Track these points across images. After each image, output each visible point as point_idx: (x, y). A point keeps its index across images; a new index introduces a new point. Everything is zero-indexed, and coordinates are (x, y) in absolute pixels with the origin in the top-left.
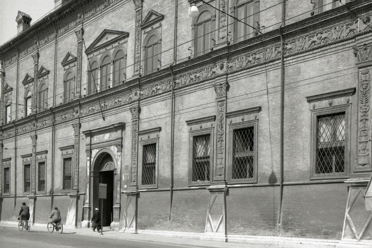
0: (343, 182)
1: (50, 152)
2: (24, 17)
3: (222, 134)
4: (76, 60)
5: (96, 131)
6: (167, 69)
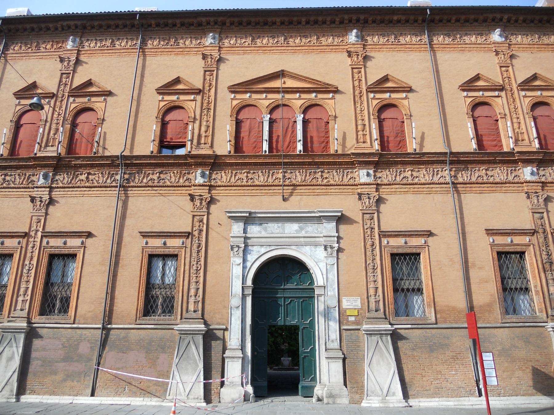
0: (173, 329)
4: (52, 97)
5: (240, 215)
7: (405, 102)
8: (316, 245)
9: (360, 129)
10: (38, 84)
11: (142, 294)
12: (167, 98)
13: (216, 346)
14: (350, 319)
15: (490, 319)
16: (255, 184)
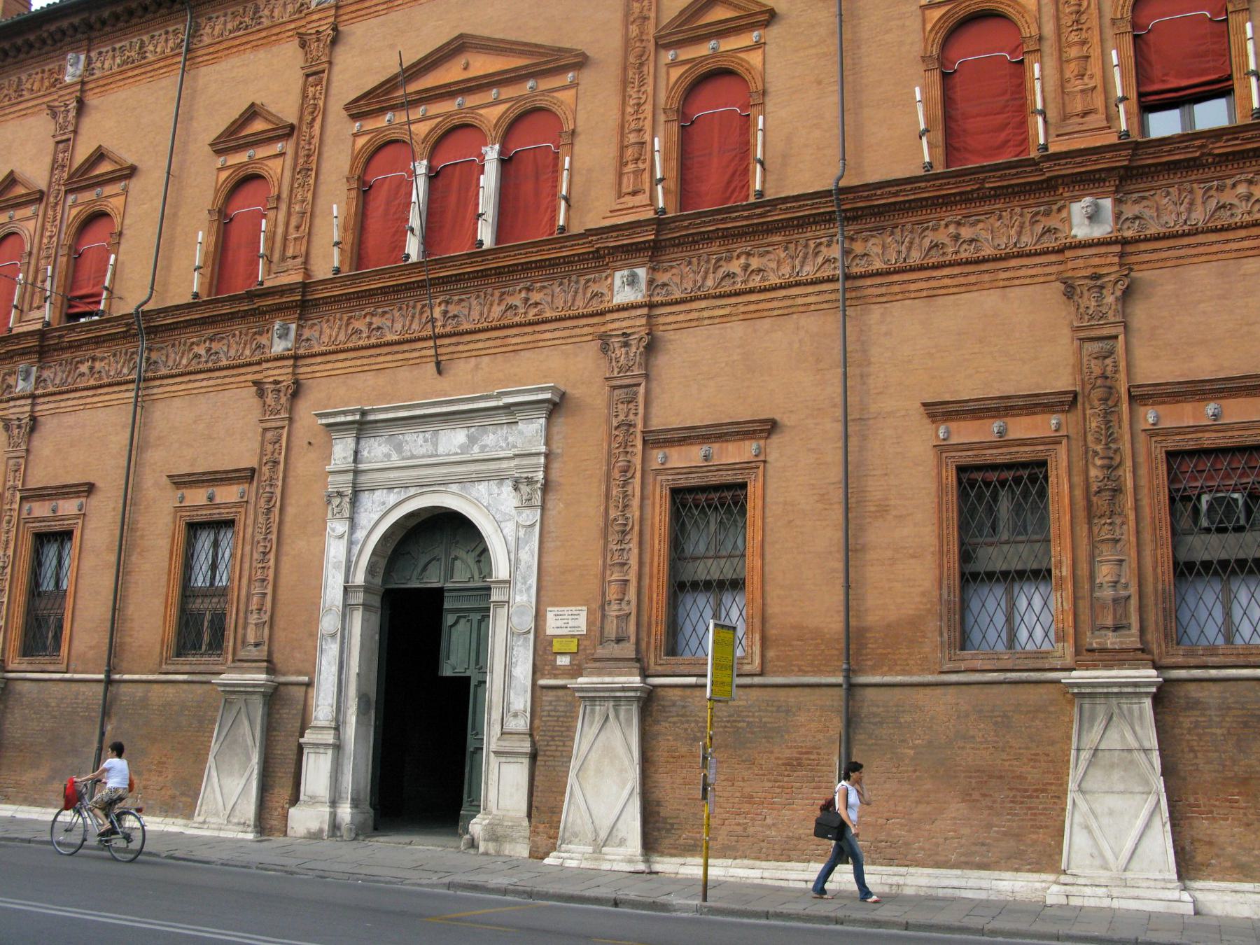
0: (209, 682)
4: (40, 200)
7: (755, 59)
8: (501, 480)
9: (630, 154)
10: (16, 176)
11: (174, 611)
12: (370, 124)
13: (288, 716)
14: (559, 663)
15: (911, 662)
16: (460, 329)
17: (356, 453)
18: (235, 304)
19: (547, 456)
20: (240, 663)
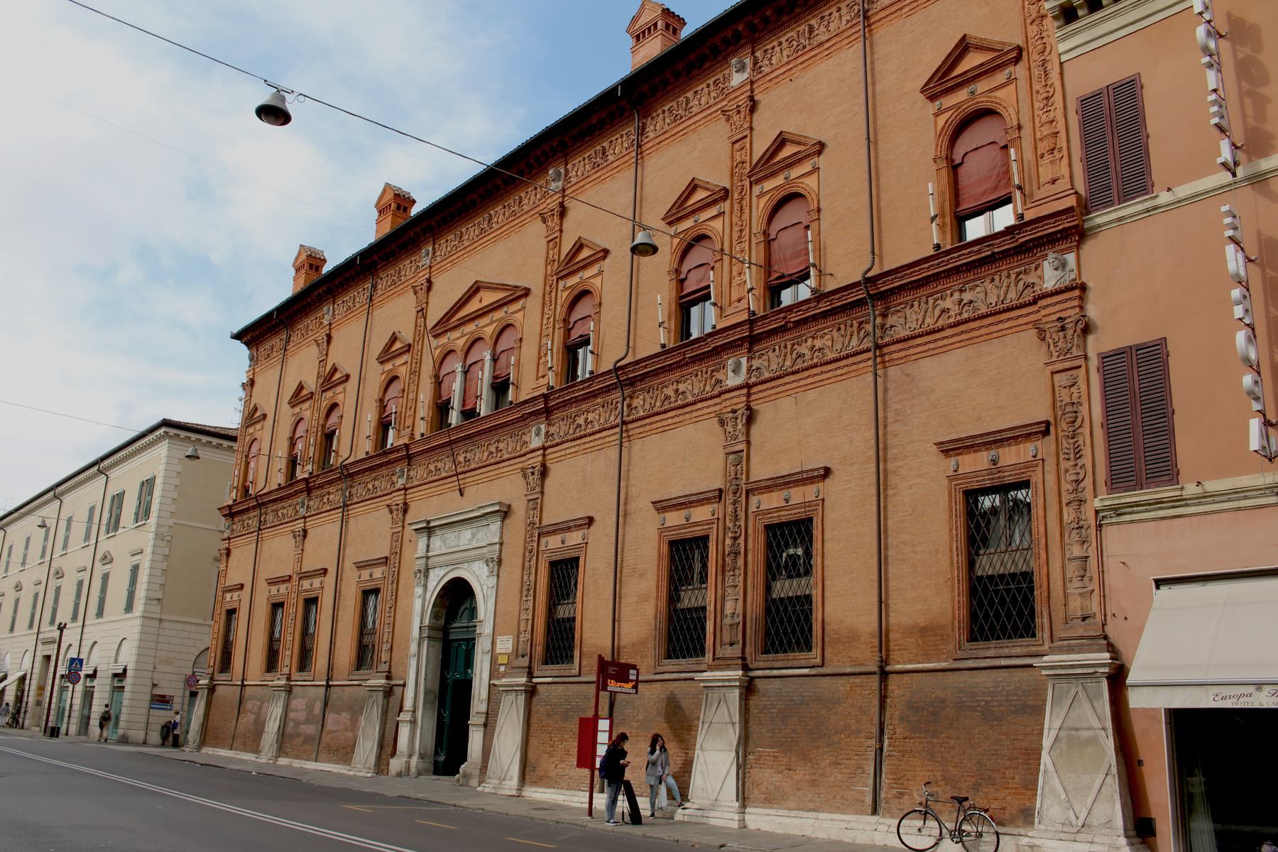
1: (247, 589)
2: (397, 196)
3: (1081, 477)
6: (609, 372)
11: (355, 643)
12: (950, 100)
17: (428, 546)
18: (385, 457)
19: (501, 544)
20: (720, 663)
